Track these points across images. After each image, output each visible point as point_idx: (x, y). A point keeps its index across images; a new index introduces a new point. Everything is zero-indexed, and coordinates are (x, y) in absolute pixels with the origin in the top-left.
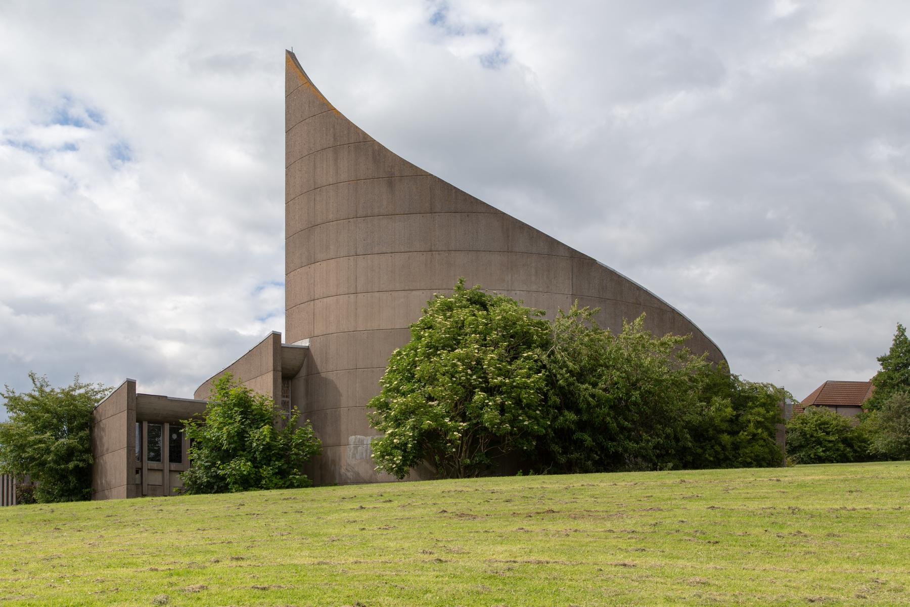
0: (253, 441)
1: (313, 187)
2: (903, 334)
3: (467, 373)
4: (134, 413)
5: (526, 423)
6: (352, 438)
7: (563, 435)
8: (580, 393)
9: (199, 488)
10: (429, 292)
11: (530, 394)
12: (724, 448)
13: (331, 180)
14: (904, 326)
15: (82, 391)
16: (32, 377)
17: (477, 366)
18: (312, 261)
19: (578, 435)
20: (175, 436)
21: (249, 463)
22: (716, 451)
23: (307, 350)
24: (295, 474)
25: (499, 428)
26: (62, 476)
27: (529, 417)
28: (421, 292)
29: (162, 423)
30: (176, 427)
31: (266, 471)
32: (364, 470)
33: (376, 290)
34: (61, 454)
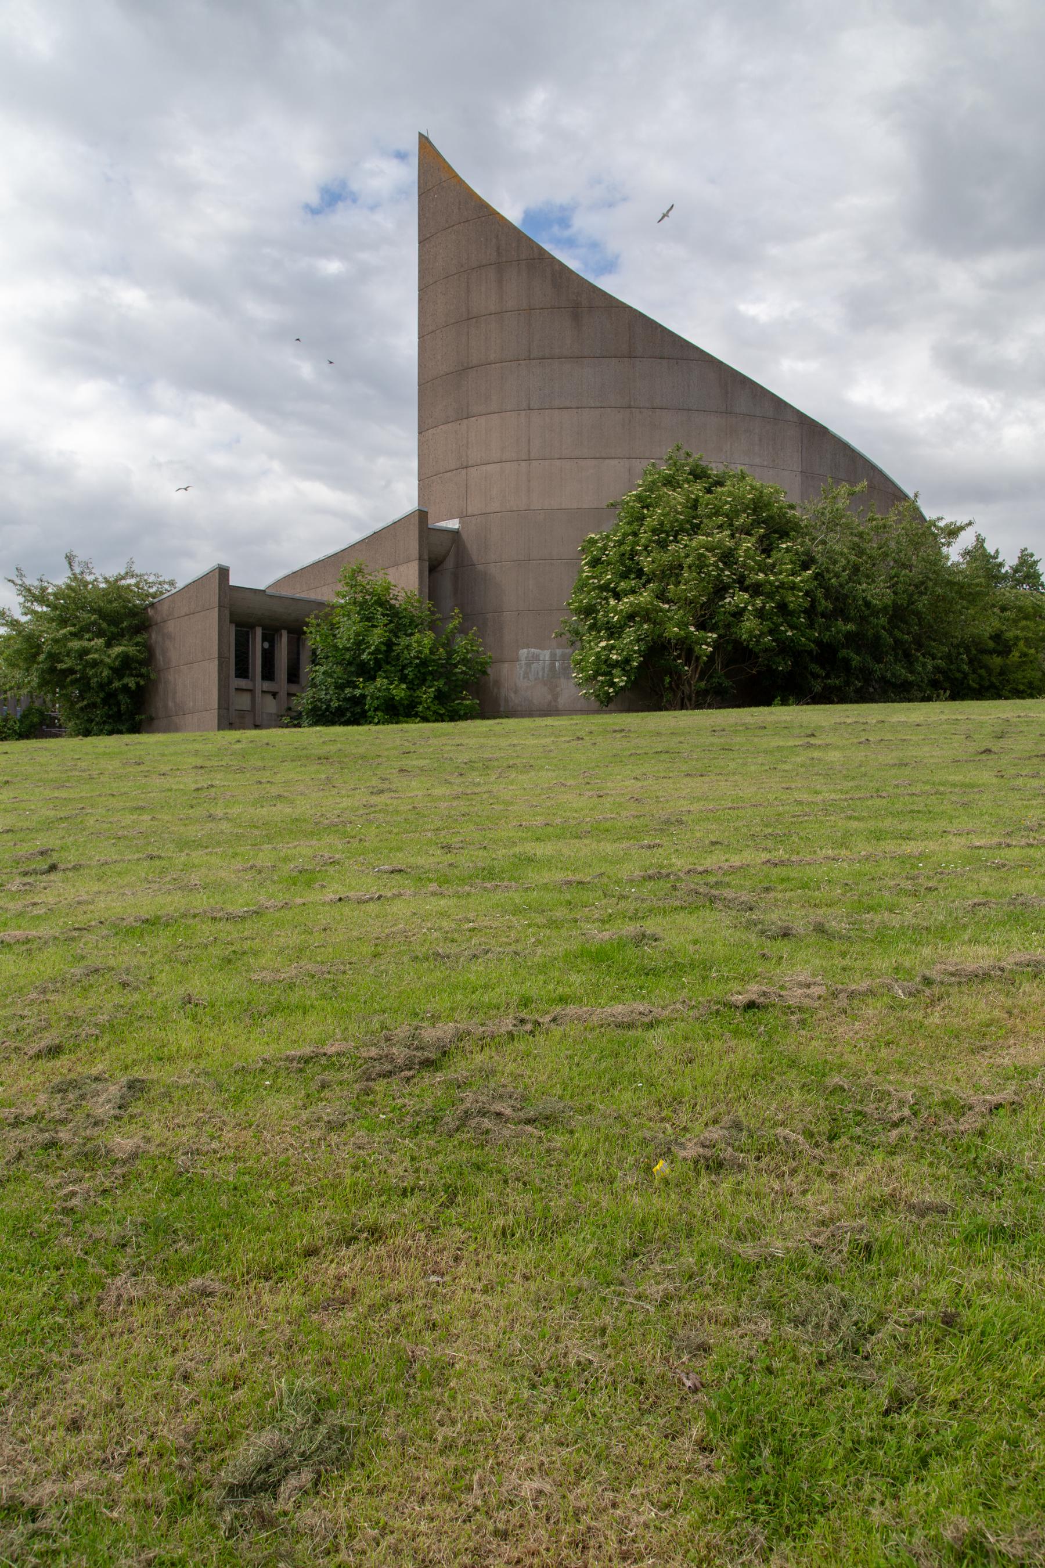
0: (360, 656)
2: (982, 546)
3: (717, 567)
4: (227, 613)
5: (789, 633)
7: (827, 654)
8: (801, 602)
9: (324, 716)
11: (798, 597)
14: (983, 535)
15: (132, 581)
17: (728, 557)
18: (464, 415)
19: (843, 653)
21: (404, 686)
22: (980, 676)
23: (456, 533)
24: (464, 699)
25: (758, 641)
28: (616, 461)
29: (252, 627)
30: (297, 632)
31: (427, 694)
32: (539, 695)
33: (557, 456)
34: (101, 664)
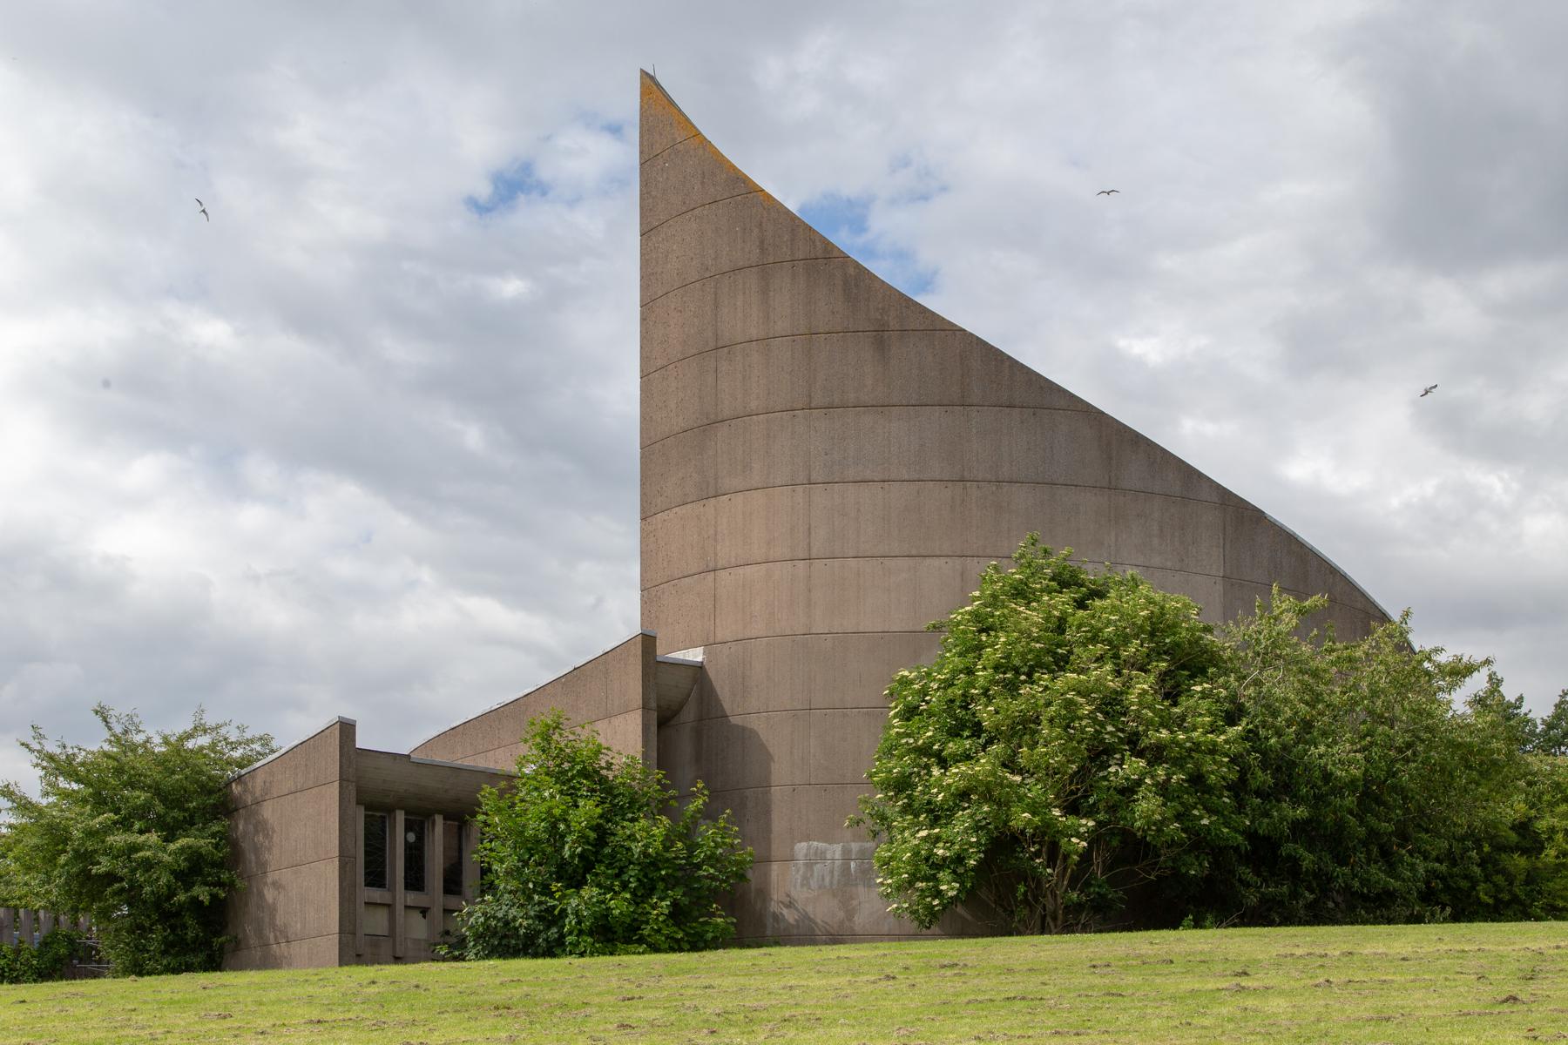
1: (712, 345)
3: (1095, 720)
4: (352, 789)
5: (1205, 822)
6: (801, 847)
9: (504, 942)
10: (958, 561)
12: (1510, 879)
13: (754, 333)
15: (204, 740)
16: (102, 714)
19: (1288, 848)
20: (412, 837)
23: (699, 668)
25: (1159, 830)
26: (164, 911)
27: (1210, 811)
29: (390, 810)
32: (824, 911)
34: (160, 863)
